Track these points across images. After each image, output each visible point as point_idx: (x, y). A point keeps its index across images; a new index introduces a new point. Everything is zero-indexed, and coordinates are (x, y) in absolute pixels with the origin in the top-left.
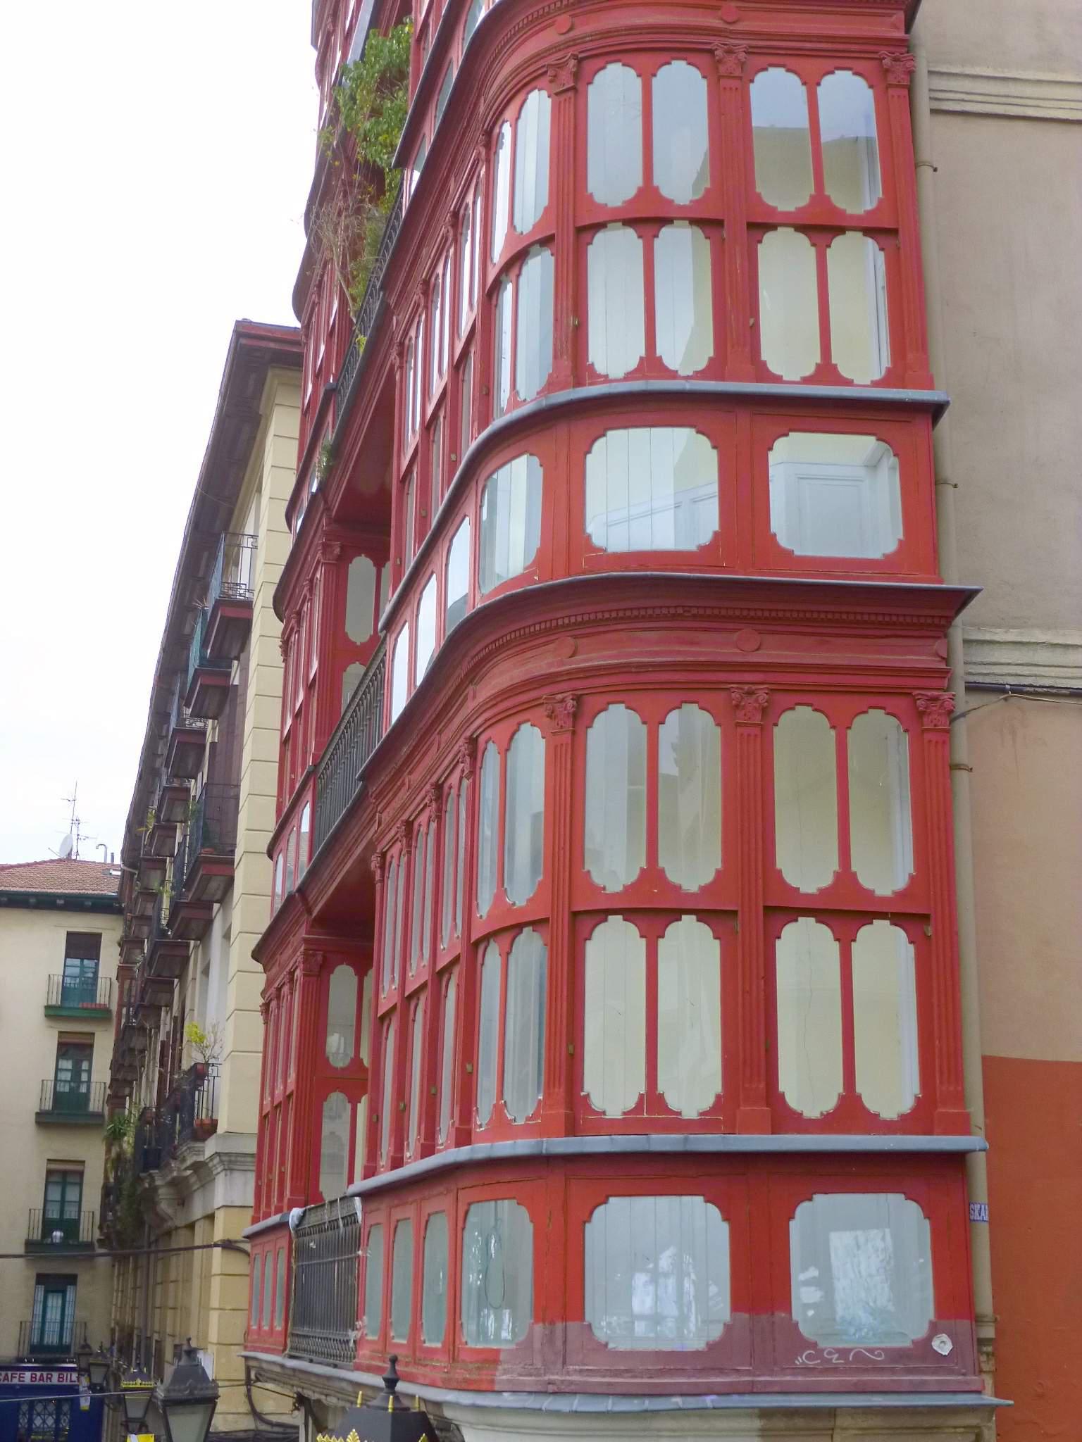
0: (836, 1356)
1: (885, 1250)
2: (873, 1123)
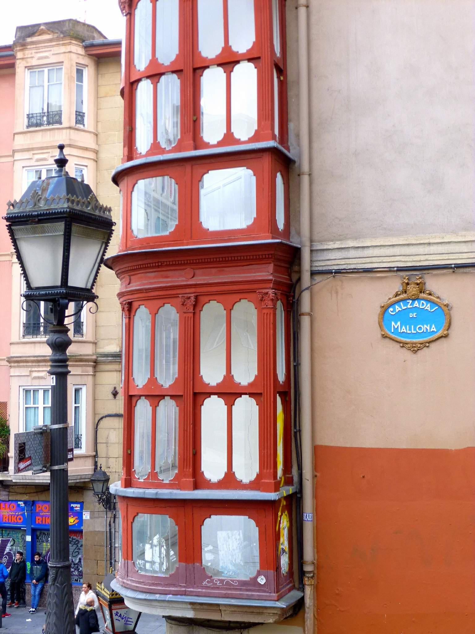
0: (219, 582)
1: (240, 539)
2: (239, 485)
